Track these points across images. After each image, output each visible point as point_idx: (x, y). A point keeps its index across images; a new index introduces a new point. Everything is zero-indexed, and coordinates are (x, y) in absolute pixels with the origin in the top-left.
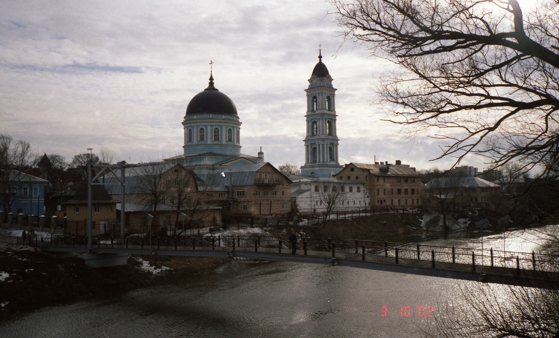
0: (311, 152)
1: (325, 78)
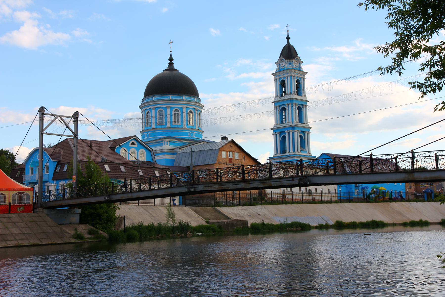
0: (280, 141)
1: (294, 60)
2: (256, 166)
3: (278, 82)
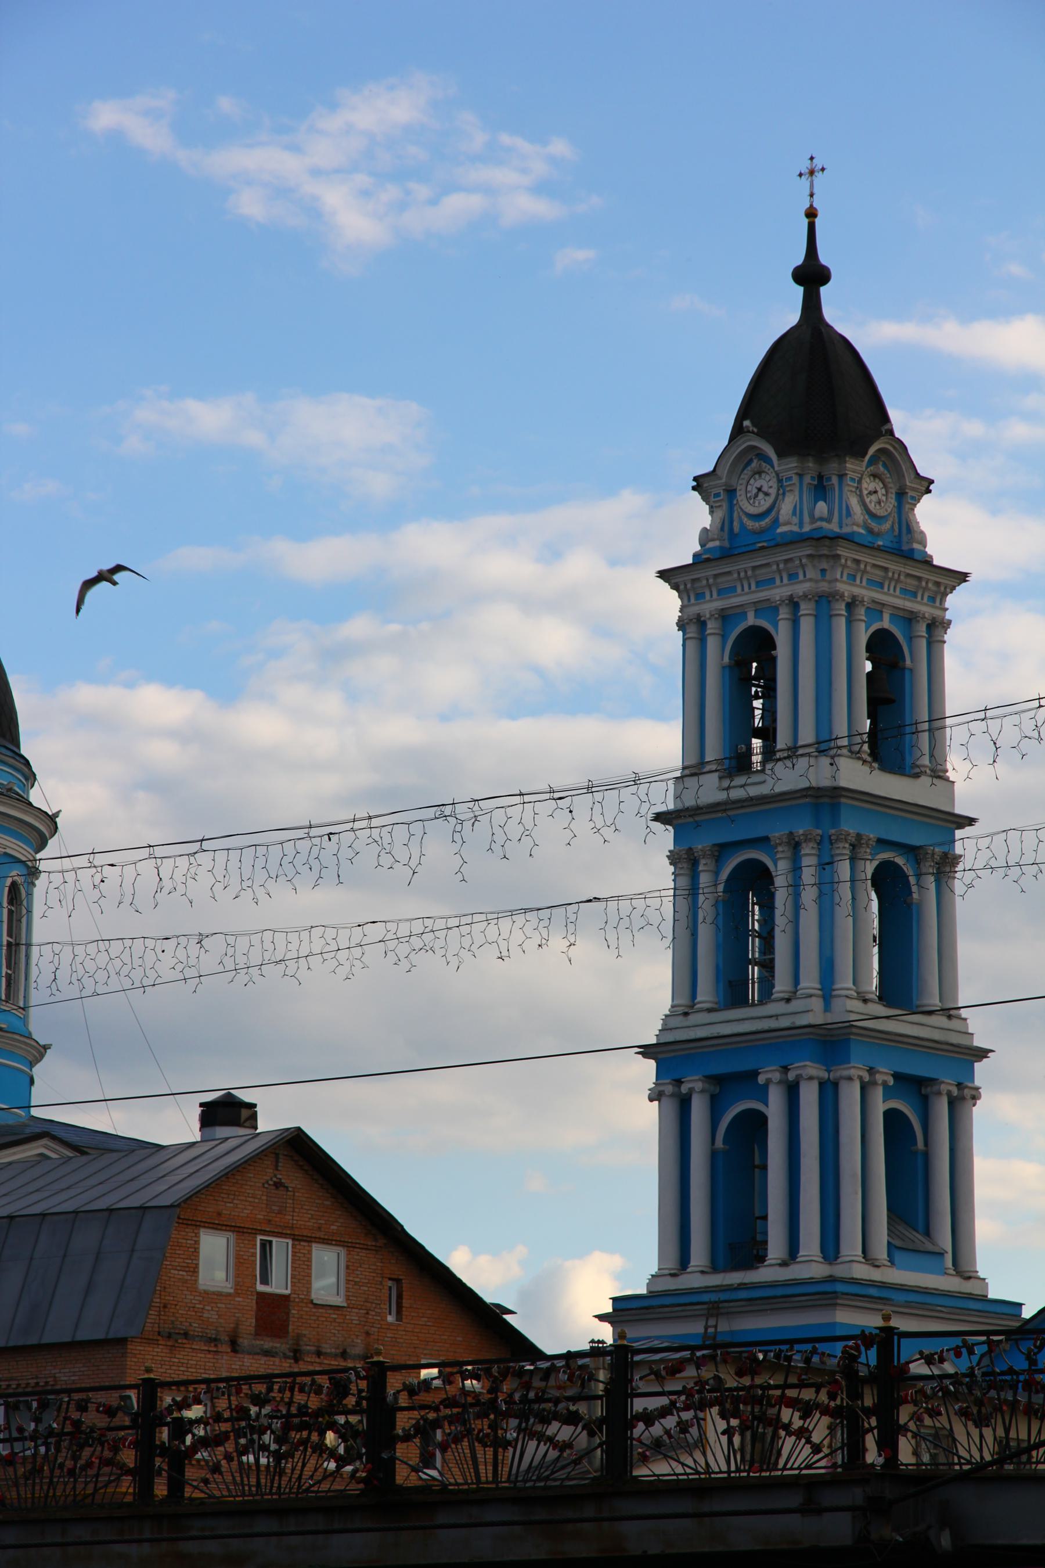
0: (714, 1155)
1: (853, 466)
2: (488, 1372)
3: (712, 644)
